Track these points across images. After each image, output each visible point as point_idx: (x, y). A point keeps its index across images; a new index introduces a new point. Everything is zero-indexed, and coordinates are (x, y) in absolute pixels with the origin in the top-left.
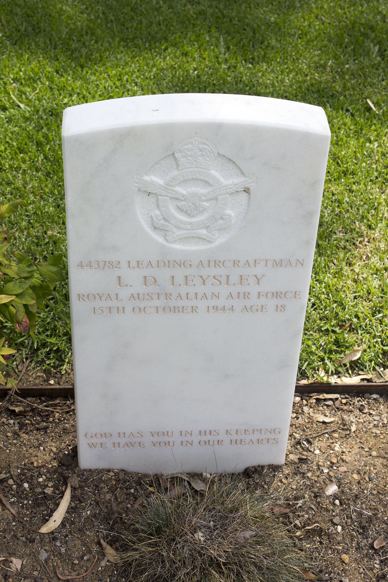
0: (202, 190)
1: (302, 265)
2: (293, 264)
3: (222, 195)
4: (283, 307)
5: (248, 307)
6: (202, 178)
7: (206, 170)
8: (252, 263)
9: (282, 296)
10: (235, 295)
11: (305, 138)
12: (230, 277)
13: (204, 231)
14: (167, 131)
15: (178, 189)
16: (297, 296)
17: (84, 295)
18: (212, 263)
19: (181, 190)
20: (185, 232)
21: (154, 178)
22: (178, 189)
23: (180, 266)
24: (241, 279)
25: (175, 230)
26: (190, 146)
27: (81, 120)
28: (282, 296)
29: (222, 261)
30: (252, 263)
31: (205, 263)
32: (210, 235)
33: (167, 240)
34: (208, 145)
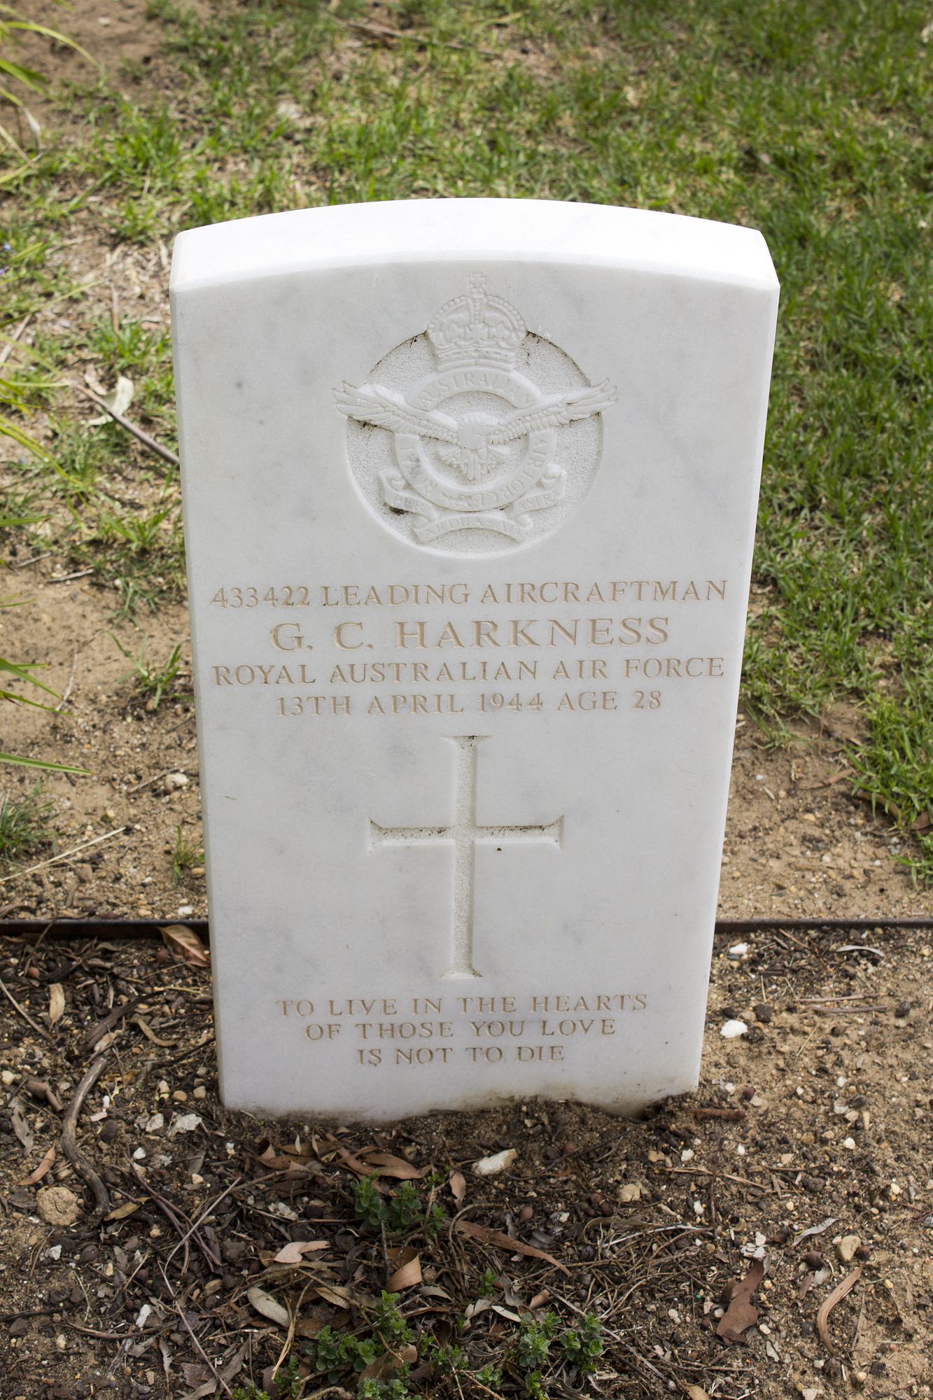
0: (485, 417)
1: (722, 593)
2: (702, 592)
3: (538, 429)
4: (656, 698)
5: (574, 696)
6: (490, 388)
7: (500, 371)
8: (606, 591)
9: (233, 679)
10: (572, 668)
11: (726, 299)
12: (426, 627)
13: (499, 516)
14: (409, 279)
15: (438, 416)
16: (716, 671)
17: (228, 670)
18: (516, 592)
19: (446, 419)
20: (458, 516)
21: (384, 391)
22: (438, 416)
23: (442, 598)
24: (402, 633)
25: (435, 514)
26: (462, 316)
27: (209, 258)
28: (233, 679)
29: (538, 586)
30: (606, 591)
31: (501, 593)
32: (513, 522)
33: (416, 538)
34: (505, 314)
